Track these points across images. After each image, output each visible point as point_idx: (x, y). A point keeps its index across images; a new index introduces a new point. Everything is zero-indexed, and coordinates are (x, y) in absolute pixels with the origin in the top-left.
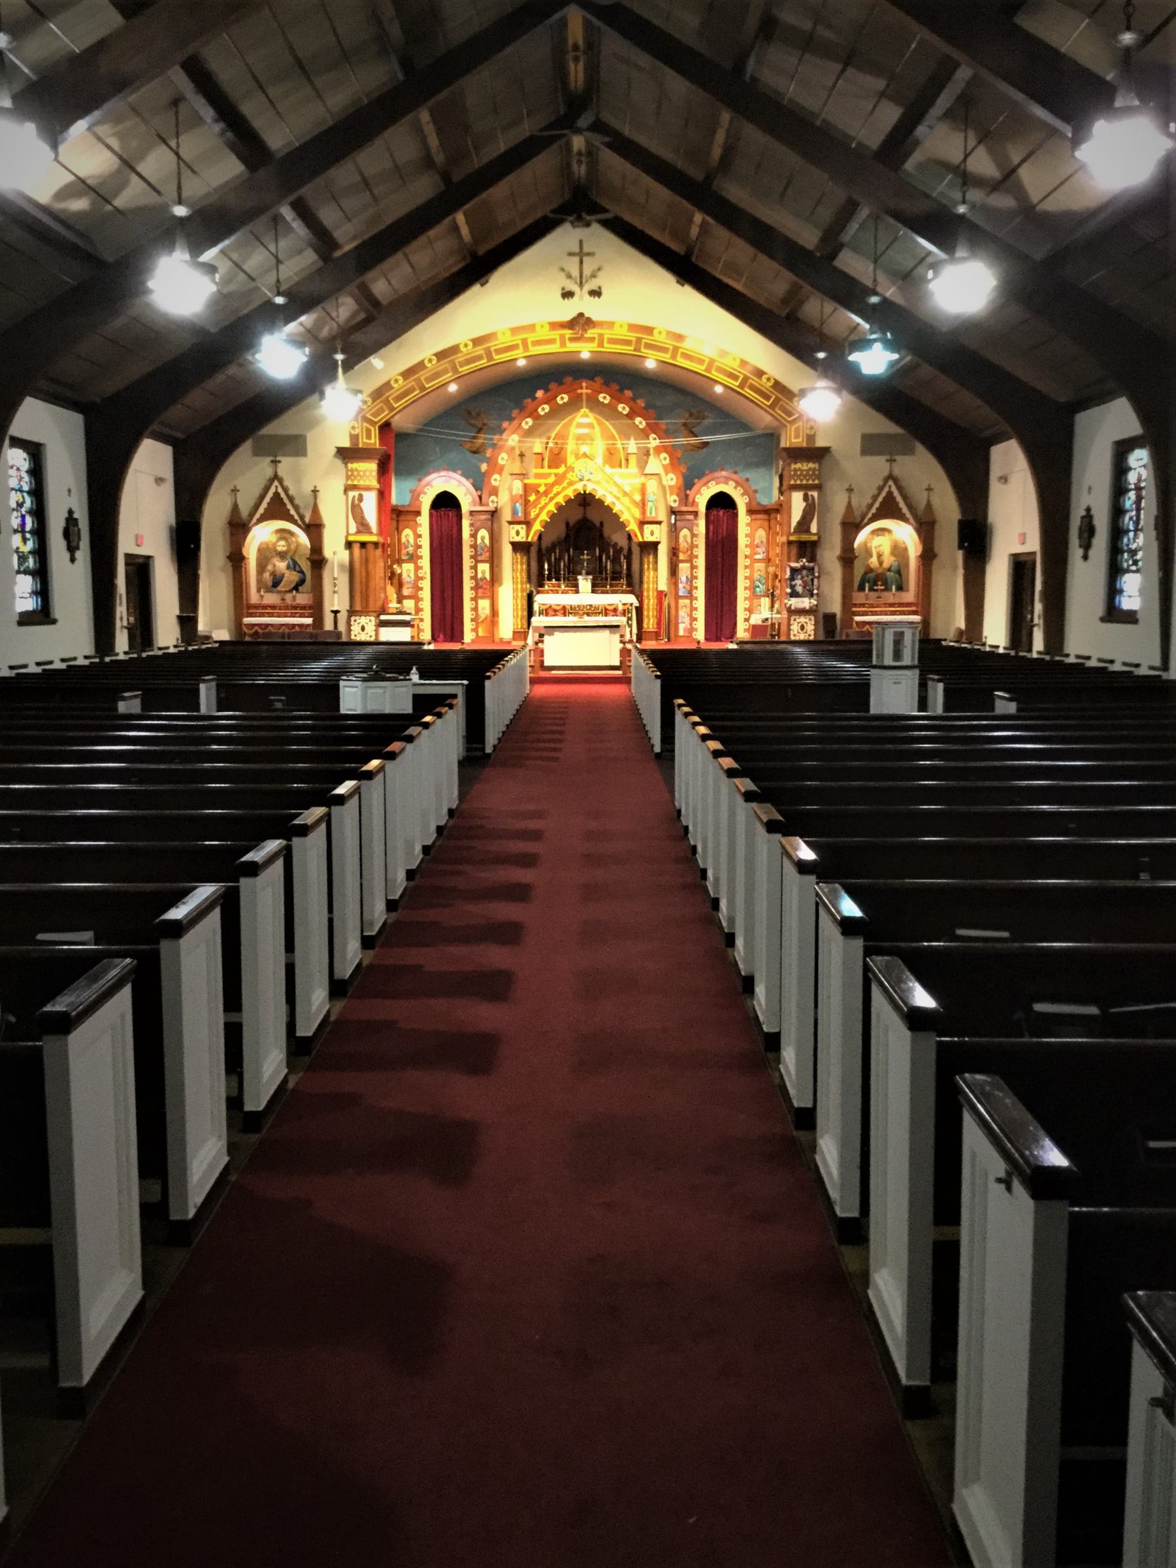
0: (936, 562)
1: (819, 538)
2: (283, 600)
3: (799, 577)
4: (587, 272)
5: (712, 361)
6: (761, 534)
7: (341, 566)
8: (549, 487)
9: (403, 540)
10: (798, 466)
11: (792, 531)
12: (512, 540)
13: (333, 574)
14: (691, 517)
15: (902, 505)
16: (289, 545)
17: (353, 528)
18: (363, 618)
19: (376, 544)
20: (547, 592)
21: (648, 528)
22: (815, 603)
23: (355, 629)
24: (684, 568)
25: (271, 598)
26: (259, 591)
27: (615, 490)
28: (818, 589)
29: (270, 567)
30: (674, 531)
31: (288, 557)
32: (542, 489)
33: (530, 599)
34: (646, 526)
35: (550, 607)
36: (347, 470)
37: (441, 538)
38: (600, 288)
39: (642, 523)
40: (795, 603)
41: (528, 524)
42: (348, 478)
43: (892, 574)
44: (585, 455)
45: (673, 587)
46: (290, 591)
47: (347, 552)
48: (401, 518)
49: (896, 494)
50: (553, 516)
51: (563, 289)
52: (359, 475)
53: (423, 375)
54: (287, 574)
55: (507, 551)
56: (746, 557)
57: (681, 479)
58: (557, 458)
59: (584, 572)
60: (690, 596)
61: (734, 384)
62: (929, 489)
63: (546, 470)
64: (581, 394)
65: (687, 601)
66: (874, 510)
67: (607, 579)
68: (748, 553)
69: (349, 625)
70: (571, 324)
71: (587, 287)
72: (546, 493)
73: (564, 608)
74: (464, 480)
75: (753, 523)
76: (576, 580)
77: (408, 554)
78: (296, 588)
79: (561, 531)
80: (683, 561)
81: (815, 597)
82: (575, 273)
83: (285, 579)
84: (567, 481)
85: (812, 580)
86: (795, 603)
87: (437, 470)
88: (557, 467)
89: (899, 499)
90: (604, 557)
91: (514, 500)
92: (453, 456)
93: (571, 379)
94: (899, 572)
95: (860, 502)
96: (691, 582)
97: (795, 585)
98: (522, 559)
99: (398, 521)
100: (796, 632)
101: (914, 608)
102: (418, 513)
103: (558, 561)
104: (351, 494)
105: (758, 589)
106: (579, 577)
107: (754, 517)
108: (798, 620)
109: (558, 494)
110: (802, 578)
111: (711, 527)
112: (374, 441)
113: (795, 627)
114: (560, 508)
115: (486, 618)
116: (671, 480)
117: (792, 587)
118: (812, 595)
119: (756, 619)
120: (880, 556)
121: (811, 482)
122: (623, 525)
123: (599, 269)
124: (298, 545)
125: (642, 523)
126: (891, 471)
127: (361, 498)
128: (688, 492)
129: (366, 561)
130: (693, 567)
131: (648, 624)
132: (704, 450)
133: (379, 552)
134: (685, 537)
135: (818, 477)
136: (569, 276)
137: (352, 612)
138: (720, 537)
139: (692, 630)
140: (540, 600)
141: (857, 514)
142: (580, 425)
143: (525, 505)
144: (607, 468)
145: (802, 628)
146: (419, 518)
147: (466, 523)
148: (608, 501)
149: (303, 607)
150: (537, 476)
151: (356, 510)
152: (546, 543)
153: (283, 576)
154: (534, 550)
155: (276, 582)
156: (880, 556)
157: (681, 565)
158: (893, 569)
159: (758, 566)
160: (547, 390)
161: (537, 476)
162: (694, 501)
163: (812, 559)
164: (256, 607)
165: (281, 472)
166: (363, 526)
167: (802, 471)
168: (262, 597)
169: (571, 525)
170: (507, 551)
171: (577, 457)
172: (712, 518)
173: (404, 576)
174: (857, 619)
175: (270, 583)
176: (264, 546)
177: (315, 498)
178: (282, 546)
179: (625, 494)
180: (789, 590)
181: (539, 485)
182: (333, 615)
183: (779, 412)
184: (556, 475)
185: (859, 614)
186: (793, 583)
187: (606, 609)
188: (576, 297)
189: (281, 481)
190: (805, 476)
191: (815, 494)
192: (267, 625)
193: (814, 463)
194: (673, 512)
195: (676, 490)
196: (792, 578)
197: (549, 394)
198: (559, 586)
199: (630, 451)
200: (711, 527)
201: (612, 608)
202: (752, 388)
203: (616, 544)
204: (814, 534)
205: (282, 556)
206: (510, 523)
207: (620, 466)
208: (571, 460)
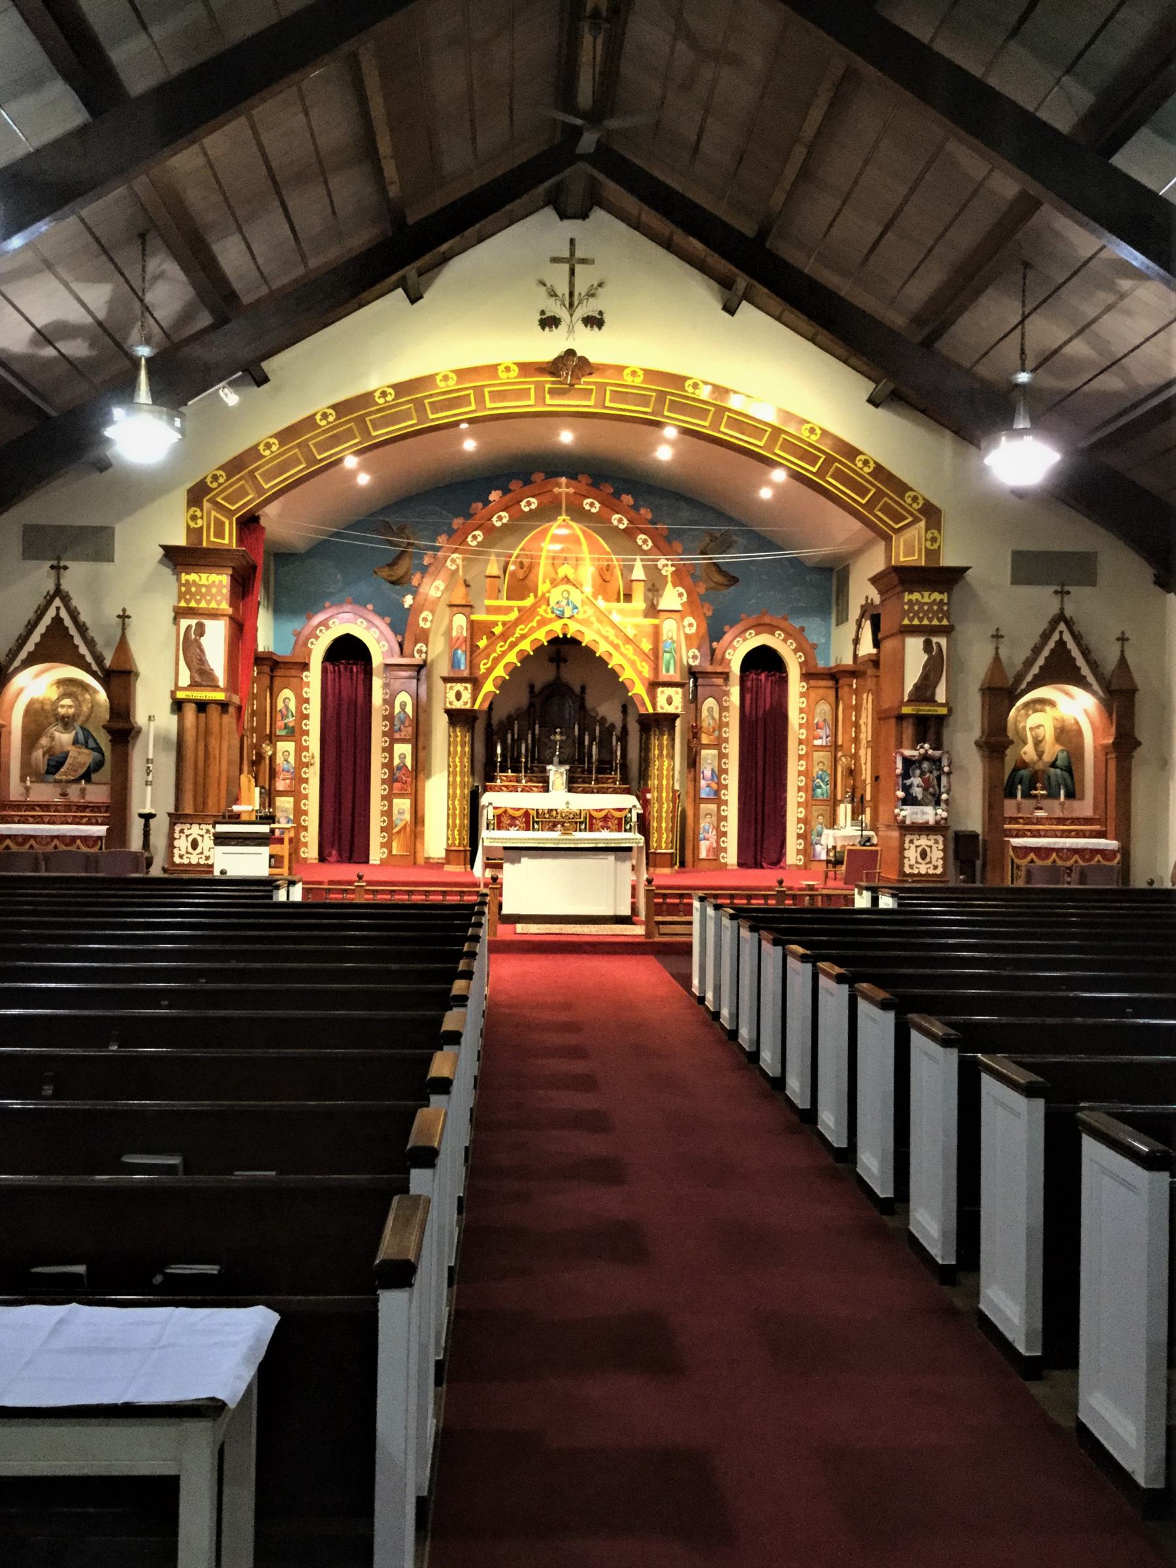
0: (1138, 753)
1: (950, 710)
2: (64, 795)
3: (918, 772)
4: (581, 288)
5: (777, 431)
6: (823, 709)
7: (161, 740)
8: (509, 628)
9: (280, 705)
10: (916, 596)
11: (906, 699)
12: (449, 706)
13: (147, 753)
14: (720, 681)
15: (1080, 662)
16: (79, 705)
17: (185, 678)
18: (195, 827)
19: (224, 706)
20: (500, 789)
21: (663, 694)
22: (945, 815)
23: (182, 844)
24: (708, 756)
25: (44, 792)
26: (23, 779)
27: (611, 633)
28: (948, 792)
29: (44, 741)
30: (694, 701)
31: (77, 725)
32: (498, 630)
33: (475, 797)
34: (660, 690)
35: (505, 812)
36: (181, 585)
37: (340, 705)
38: (601, 313)
39: (654, 686)
40: (908, 814)
41: (476, 682)
42: (181, 596)
43: (1058, 771)
44: (566, 580)
45: (691, 785)
46: (77, 781)
47: (175, 718)
48: (279, 672)
49: (1071, 645)
50: (514, 671)
51: (543, 312)
52: (198, 592)
53: (312, 439)
54: (73, 752)
55: (440, 724)
56: (801, 742)
57: (704, 626)
58: (521, 585)
59: (556, 759)
60: (718, 800)
61: (810, 470)
62: (1123, 639)
63: (504, 602)
64: (560, 493)
65: (713, 807)
66: (1035, 670)
67: (591, 773)
68: (803, 737)
69: (171, 838)
70: (554, 368)
71: (581, 312)
72: (504, 636)
73: (526, 814)
74: (377, 620)
75: (813, 694)
76: (544, 770)
77: (286, 726)
78: (87, 776)
79: (523, 700)
80: (708, 747)
81: (943, 805)
82: (563, 289)
83: (69, 761)
84: (538, 618)
85: (939, 778)
86: (908, 814)
87: (339, 603)
88: (523, 597)
89: (1075, 653)
90: (587, 737)
91: (452, 645)
92: (364, 587)
93: (542, 476)
94: (1069, 769)
95: (1015, 655)
96: (719, 778)
97: (911, 785)
98: (463, 737)
99: (272, 678)
100: (913, 862)
101: (1097, 827)
102: (305, 666)
103: (517, 742)
104: (184, 623)
105: (819, 791)
106: (549, 767)
107: (813, 683)
108: (917, 843)
109: (523, 637)
110: (922, 775)
111: (748, 697)
112: (229, 539)
113: (912, 854)
114: (525, 659)
115: (404, 827)
116: (691, 625)
117: (906, 789)
118: (937, 803)
119: (829, 839)
120: (1038, 743)
121: (935, 622)
122: (623, 688)
123: (600, 285)
124: (94, 704)
125: (654, 686)
126: (1062, 609)
127: (201, 630)
128: (715, 644)
129: (205, 734)
130: (722, 756)
131: (659, 840)
132: (732, 588)
133: (229, 720)
134: (710, 710)
135: (947, 615)
136: (553, 294)
137: (176, 818)
138: (761, 713)
139: (719, 850)
140: (493, 801)
141: (1011, 674)
142: (556, 539)
143: (472, 653)
144: (601, 603)
145: (924, 855)
146: (305, 673)
147: (377, 683)
148: (601, 649)
149: (95, 808)
150: (490, 610)
151: (191, 649)
152: (499, 715)
153: (66, 755)
154: (480, 726)
155: (56, 763)
156: (1038, 743)
157: (704, 753)
158: (1059, 763)
159: (818, 756)
160: (506, 491)
161: (490, 610)
162: (723, 657)
163: (937, 746)
164: (17, 806)
165: (68, 583)
166: (203, 675)
167: (922, 605)
168: (27, 789)
169: (538, 688)
170: (440, 724)
171: (554, 583)
172: (749, 684)
173: (280, 759)
174: (1016, 842)
175: (43, 767)
176: (37, 706)
177: (124, 629)
178: (66, 706)
179: (628, 640)
180: (900, 794)
181: (495, 624)
182: (142, 821)
183: (879, 514)
184: (520, 609)
185: (1019, 834)
186: (908, 782)
187: (591, 817)
188: (563, 327)
189: (66, 599)
190: (926, 613)
191: (943, 641)
192: (27, 838)
193: (941, 592)
194: (693, 673)
195: (696, 642)
196: (906, 775)
197: (509, 496)
198: (519, 781)
199: (634, 577)
200: (748, 697)
201: (603, 814)
202: (839, 476)
203: (603, 719)
204: (942, 705)
205: (66, 722)
206: (446, 680)
207: (618, 600)
208: (543, 588)
